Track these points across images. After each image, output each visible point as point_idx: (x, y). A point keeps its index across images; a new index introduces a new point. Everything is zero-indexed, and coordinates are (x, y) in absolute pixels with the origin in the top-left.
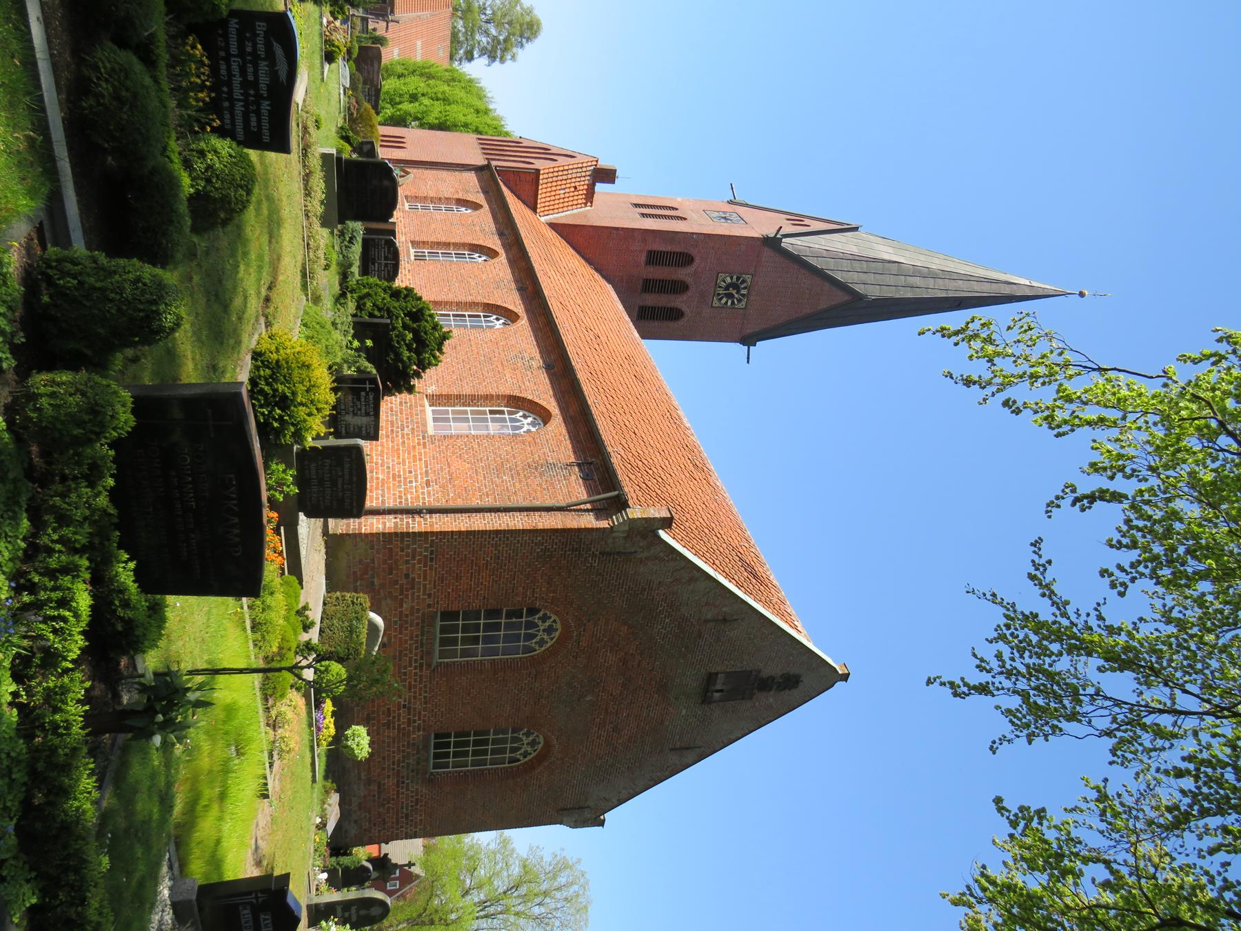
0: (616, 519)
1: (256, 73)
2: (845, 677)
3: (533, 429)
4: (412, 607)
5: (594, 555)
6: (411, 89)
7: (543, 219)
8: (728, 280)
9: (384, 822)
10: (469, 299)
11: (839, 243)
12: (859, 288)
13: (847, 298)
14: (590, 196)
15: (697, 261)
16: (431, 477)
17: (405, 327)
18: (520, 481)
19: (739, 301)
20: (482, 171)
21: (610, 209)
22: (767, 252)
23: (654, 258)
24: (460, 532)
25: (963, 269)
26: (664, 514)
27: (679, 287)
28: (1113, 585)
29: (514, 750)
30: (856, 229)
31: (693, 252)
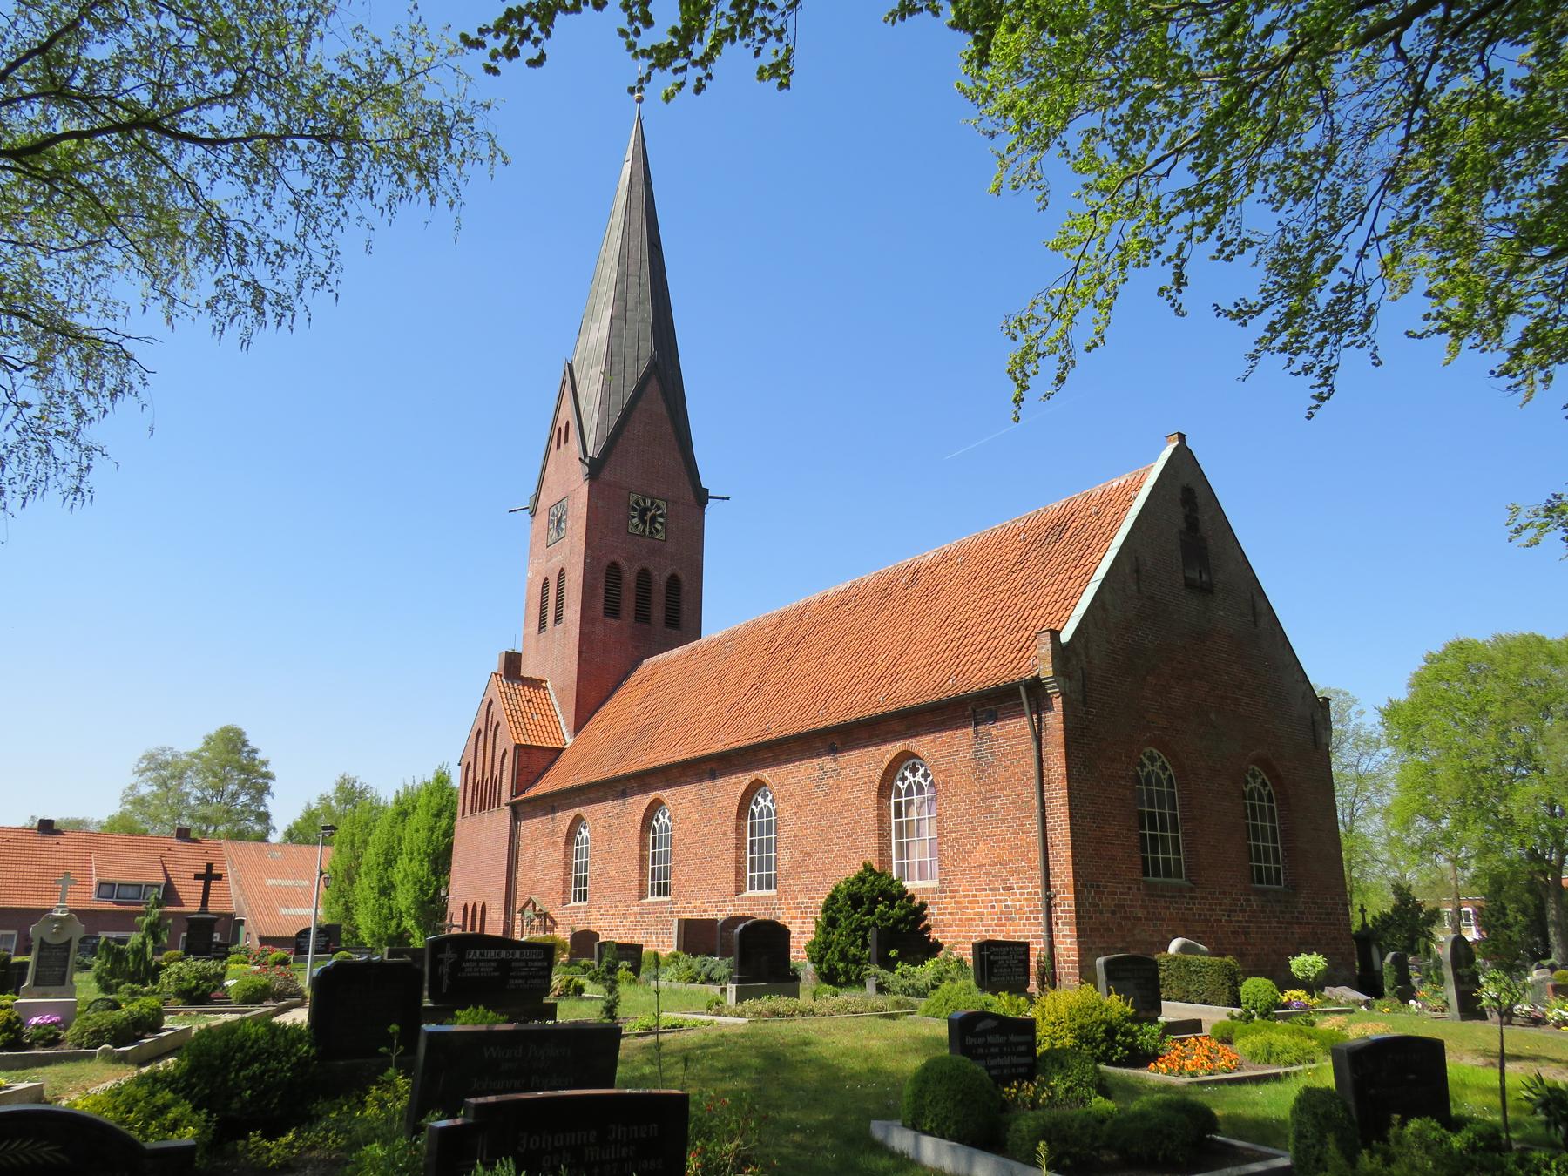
0: (1052, 689)
1: (995, 1045)
2: (1182, 437)
3: (922, 771)
5: (1087, 713)
6: (371, 896)
7: (570, 741)
8: (635, 521)
9: (1334, 938)
10: (731, 834)
11: (591, 386)
12: (643, 366)
14: (535, 684)
15: (615, 558)
16: (999, 884)
17: (871, 912)
18: (1002, 789)
19: (658, 508)
20: (519, 812)
21: (556, 660)
22: (606, 475)
23: (612, 610)
24: (1074, 856)
25: (615, 240)
26: (1046, 638)
27: (644, 577)
28: (1241, 252)
29: (1159, 783)
30: (570, 366)
31: (605, 562)
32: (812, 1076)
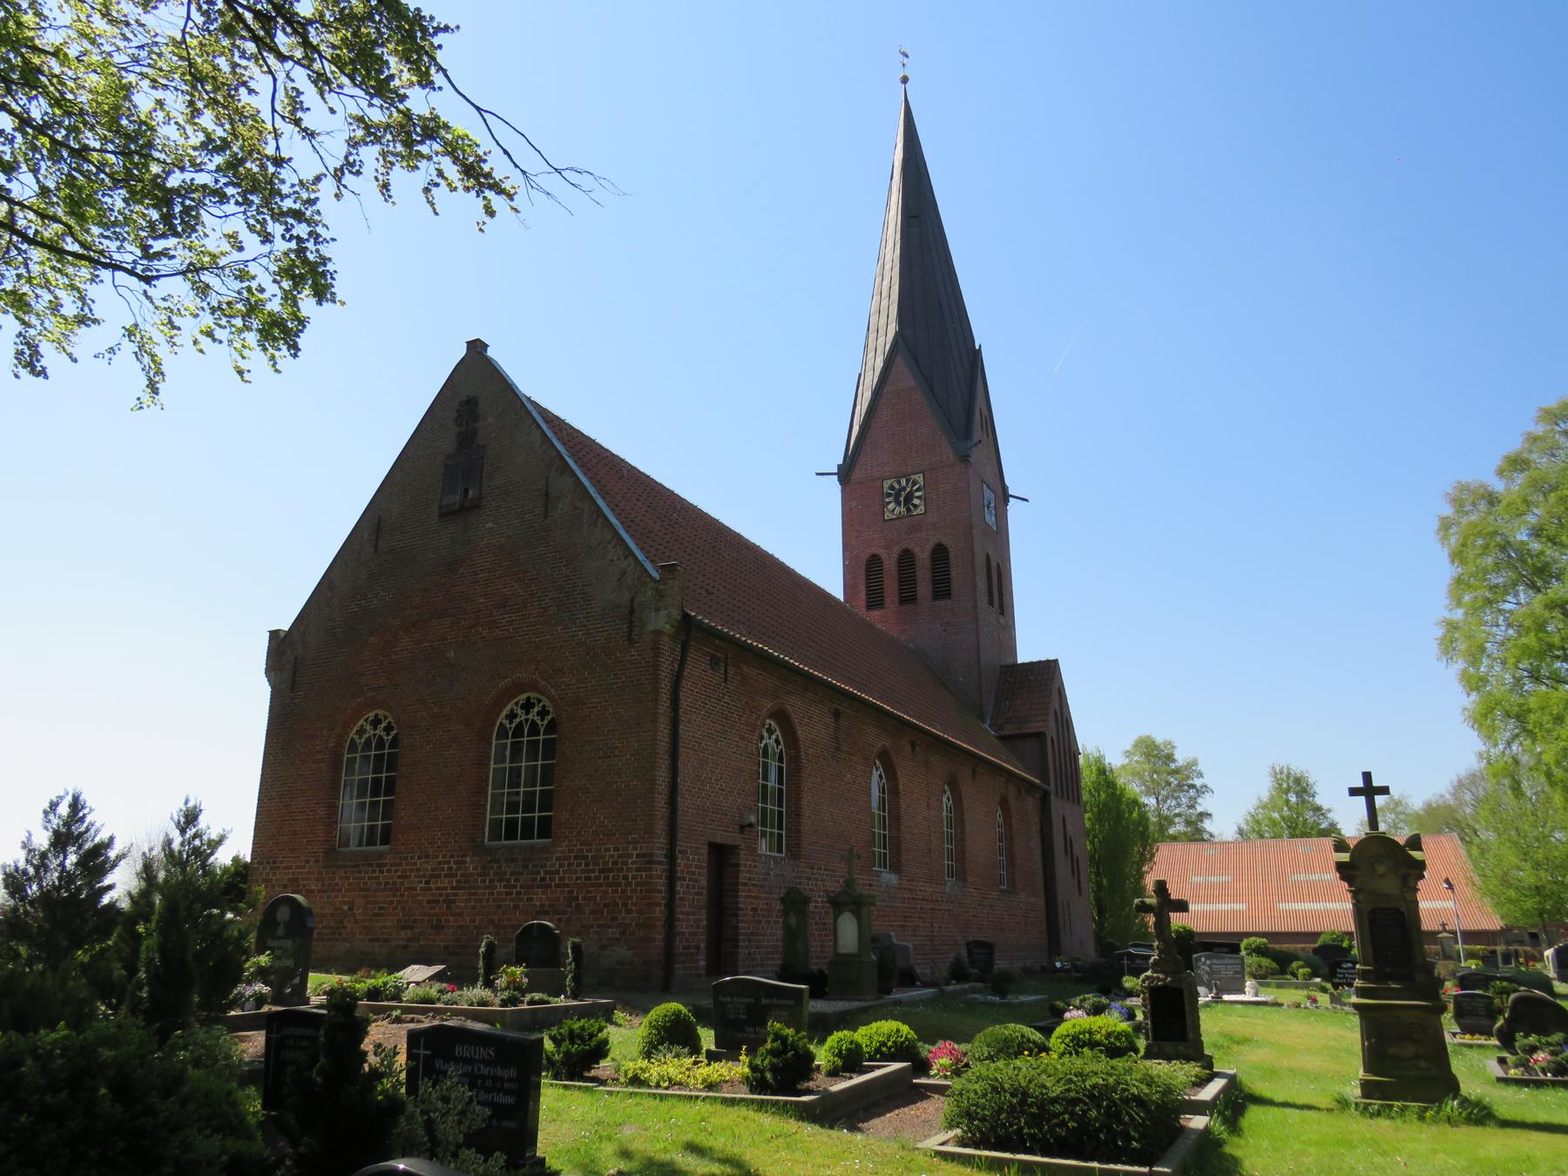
4: (317, 880)
13: (899, 360)
15: (873, 550)
22: (858, 474)
31: (864, 557)
32: (143, 884)
